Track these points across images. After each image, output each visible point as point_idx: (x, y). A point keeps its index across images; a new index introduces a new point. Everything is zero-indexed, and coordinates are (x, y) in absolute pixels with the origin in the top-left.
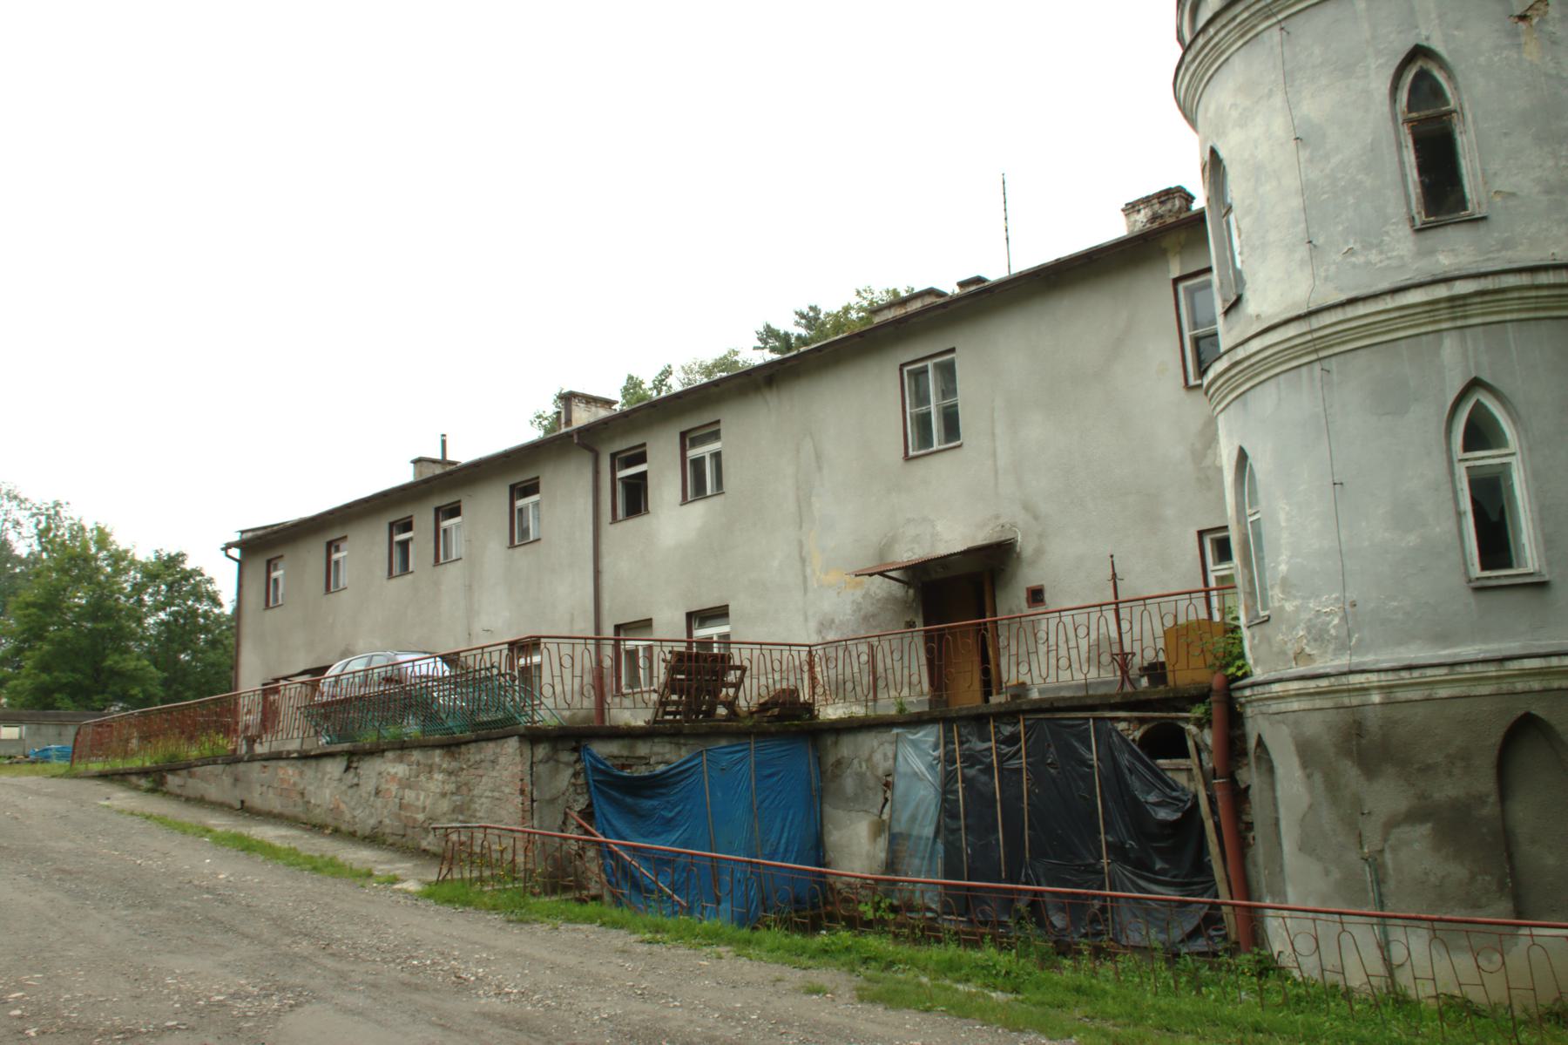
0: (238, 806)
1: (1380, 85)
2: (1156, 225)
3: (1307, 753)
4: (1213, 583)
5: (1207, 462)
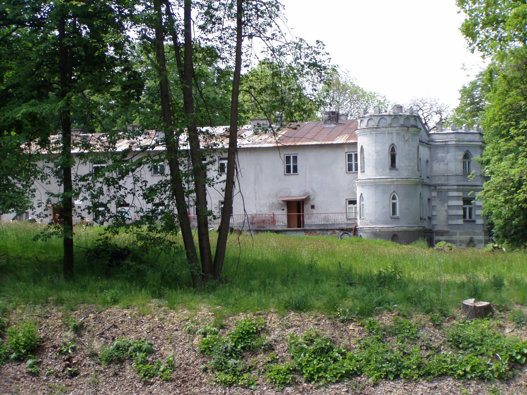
0: (282, 217)
1: (388, 148)
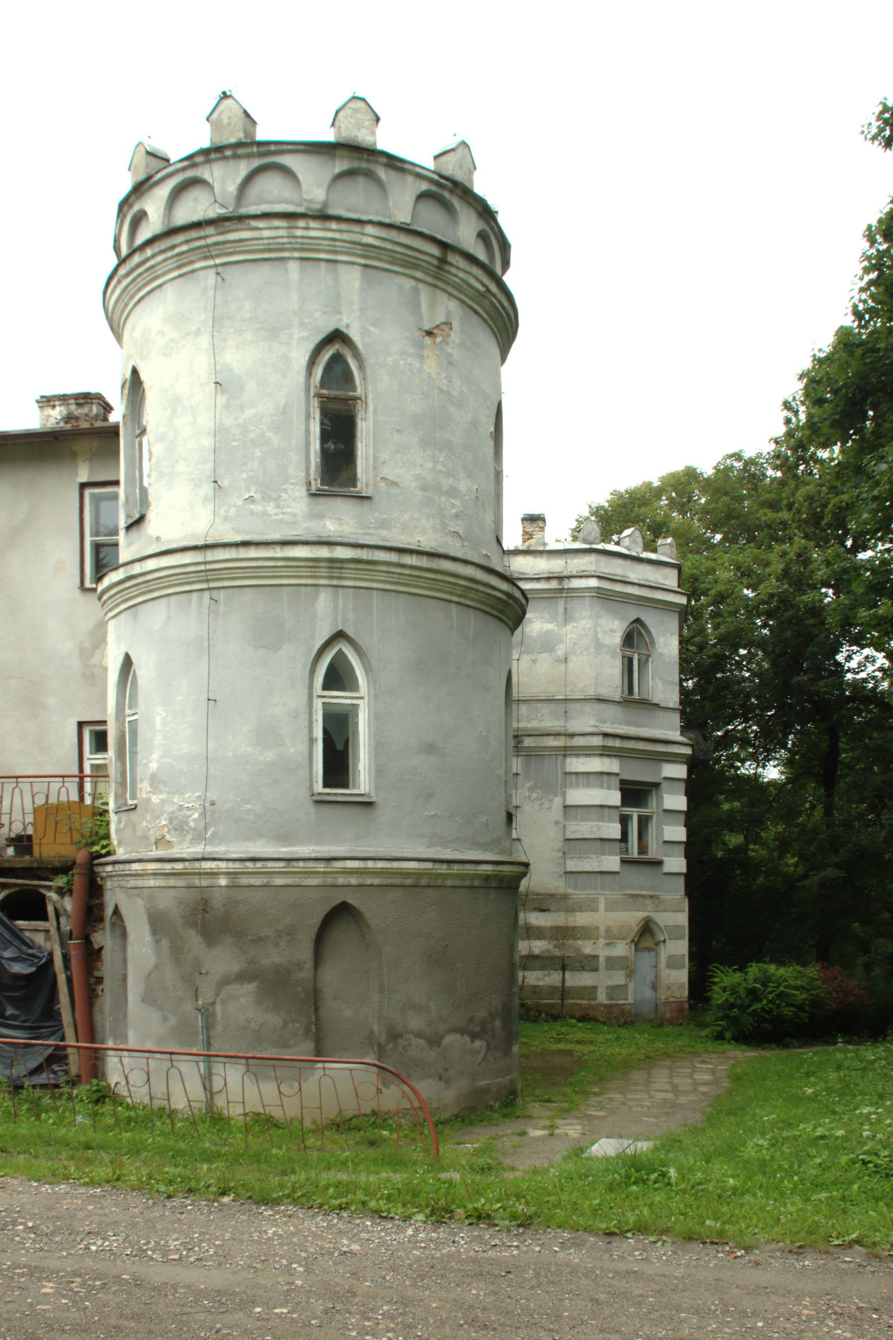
2: (68, 427)
3: (158, 923)
4: (87, 770)
5: (94, 661)
